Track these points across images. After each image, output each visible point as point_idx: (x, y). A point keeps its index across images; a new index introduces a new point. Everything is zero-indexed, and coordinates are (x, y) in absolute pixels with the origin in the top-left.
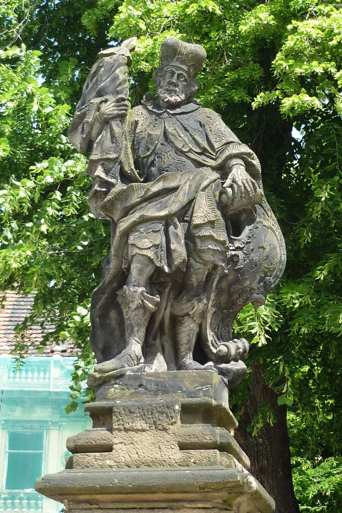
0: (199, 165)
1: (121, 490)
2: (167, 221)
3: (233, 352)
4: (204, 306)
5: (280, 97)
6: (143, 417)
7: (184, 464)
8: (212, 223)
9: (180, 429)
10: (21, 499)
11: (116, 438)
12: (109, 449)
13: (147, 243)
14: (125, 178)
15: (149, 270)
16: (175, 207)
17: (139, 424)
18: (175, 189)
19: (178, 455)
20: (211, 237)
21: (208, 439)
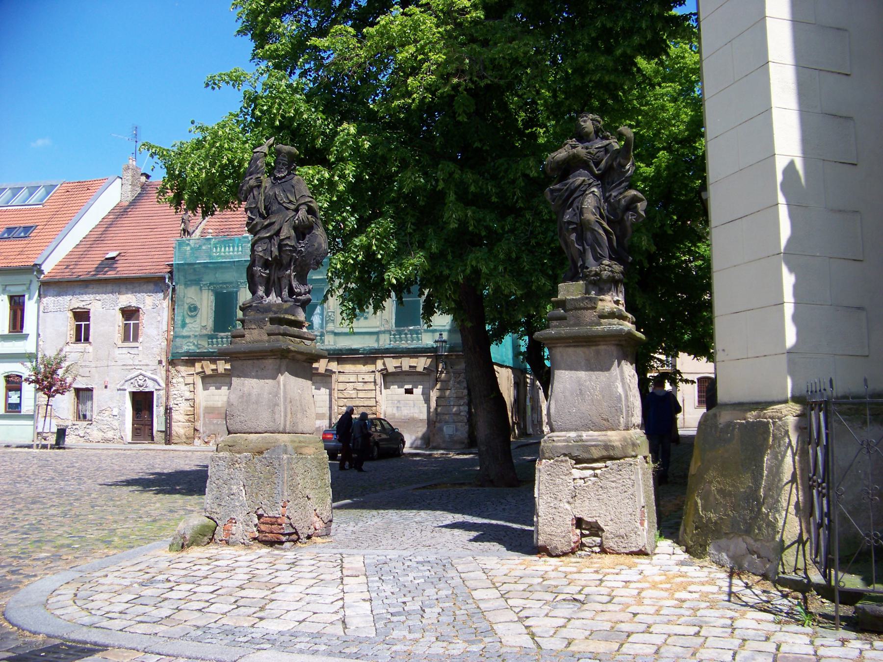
0: (287, 209)
1: (244, 353)
2: (270, 238)
3: (303, 291)
4: (291, 272)
5: (609, 25)
6: (255, 323)
7: (269, 341)
8: (288, 238)
9: (269, 327)
10: (406, 334)
11: (246, 332)
12: (243, 336)
13: (260, 249)
14: (261, 215)
15: (262, 261)
16: (272, 232)
17: (253, 327)
18: (274, 223)
19: (266, 337)
20: (287, 244)
21: (277, 332)
